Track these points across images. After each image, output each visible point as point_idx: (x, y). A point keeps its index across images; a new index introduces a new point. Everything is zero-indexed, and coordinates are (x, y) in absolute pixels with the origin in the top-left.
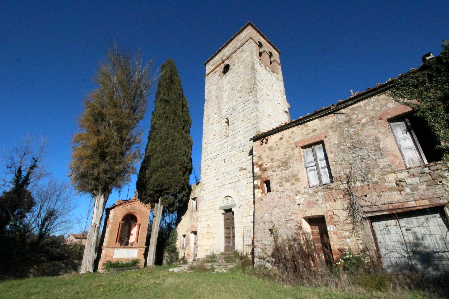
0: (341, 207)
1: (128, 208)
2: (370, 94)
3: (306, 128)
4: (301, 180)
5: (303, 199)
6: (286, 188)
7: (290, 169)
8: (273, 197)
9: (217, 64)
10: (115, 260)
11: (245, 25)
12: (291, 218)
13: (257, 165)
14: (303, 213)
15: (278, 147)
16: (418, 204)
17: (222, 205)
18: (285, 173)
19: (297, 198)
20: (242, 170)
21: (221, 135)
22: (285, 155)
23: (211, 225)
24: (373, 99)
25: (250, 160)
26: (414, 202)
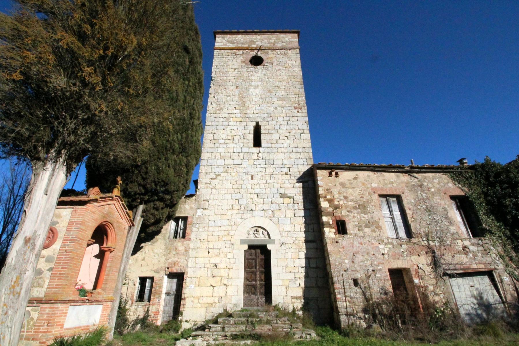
0: (425, 263)
1: (103, 211)
2: (439, 170)
6: (366, 234)
8: (352, 241)
9: (240, 45)
10: (72, 332)
11: (285, 30)
12: (379, 268)
13: (325, 199)
16: (479, 267)
17: (244, 237)
18: (364, 217)
19: (381, 246)
20: (285, 197)
24: (438, 175)
25: (299, 189)
26: (475, 265)
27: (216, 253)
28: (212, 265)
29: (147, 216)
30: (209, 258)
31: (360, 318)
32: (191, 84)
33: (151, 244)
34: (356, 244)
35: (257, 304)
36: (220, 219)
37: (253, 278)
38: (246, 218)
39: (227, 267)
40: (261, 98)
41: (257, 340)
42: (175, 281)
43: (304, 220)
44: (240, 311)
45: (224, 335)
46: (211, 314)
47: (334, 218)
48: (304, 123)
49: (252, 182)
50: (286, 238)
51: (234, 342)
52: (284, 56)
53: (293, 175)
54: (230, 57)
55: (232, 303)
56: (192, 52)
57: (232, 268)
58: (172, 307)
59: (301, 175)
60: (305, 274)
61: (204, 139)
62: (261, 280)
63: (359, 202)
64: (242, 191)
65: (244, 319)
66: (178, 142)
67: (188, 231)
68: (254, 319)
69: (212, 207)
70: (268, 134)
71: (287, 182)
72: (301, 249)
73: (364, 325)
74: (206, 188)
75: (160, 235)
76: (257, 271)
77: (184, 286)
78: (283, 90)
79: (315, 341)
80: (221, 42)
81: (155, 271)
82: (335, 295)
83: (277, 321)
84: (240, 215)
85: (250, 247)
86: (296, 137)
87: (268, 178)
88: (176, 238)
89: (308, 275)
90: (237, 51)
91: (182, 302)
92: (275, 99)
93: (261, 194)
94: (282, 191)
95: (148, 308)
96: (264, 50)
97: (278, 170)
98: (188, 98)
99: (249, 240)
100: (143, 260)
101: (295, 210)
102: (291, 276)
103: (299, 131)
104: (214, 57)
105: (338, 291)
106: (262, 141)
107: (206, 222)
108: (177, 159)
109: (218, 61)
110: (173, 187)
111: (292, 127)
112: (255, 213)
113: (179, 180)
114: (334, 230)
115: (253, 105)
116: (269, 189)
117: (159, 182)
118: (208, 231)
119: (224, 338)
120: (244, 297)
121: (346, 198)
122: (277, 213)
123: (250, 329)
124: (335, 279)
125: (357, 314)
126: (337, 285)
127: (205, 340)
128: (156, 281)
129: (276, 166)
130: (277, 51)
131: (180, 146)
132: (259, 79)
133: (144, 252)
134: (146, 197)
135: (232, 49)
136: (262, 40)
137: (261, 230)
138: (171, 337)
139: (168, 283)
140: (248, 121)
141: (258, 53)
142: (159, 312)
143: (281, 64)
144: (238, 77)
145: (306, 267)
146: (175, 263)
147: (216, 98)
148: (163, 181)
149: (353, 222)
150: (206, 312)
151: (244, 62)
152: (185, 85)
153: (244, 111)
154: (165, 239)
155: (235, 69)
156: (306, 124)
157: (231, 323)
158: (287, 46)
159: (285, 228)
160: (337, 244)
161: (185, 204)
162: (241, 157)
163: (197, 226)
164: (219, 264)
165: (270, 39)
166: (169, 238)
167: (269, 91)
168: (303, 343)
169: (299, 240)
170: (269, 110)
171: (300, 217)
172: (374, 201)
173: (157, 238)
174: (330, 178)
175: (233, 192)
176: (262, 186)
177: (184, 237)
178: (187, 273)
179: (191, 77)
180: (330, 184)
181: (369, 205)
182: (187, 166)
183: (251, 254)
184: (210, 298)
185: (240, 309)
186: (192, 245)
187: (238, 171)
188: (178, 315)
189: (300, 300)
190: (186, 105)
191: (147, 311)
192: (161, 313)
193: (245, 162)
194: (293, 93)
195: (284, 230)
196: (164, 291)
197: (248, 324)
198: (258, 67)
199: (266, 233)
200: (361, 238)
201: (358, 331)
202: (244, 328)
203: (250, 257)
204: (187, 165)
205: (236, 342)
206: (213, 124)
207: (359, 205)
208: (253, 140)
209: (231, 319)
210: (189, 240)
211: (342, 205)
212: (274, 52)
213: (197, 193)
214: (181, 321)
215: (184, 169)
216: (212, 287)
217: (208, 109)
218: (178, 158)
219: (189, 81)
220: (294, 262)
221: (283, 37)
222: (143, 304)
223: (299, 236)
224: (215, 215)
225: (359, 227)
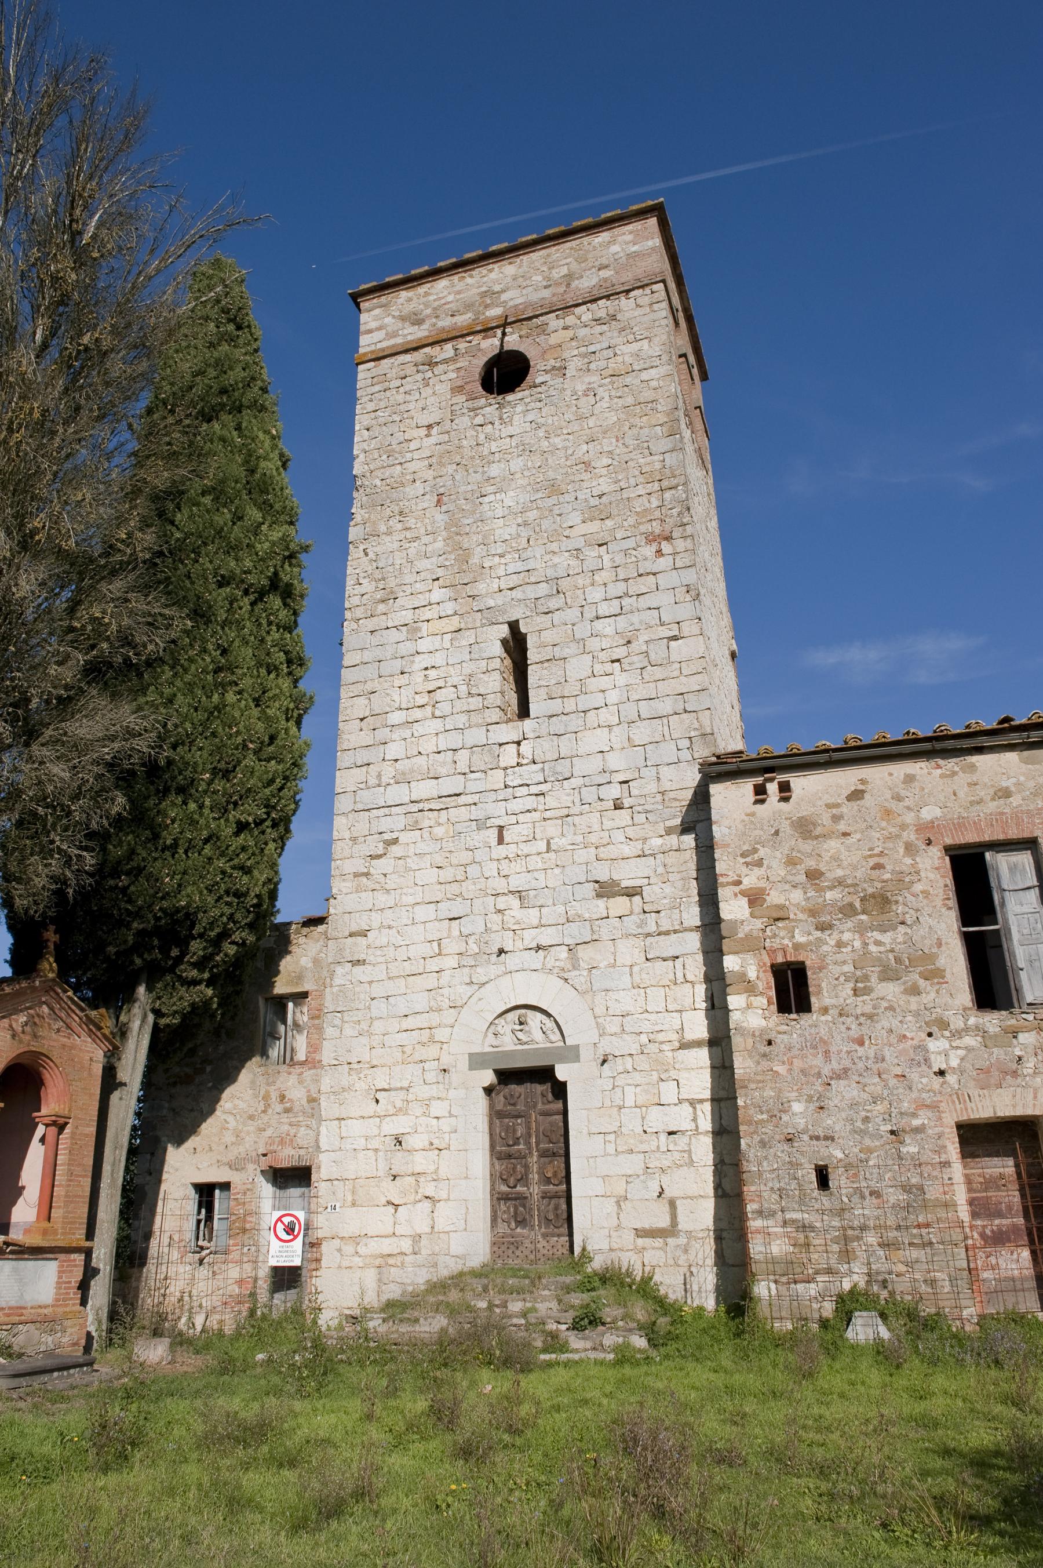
3: (969, 778)
4: (948, 976)
5: (961, 1053)
7: (901, 929)
9: (446, 322)
12: (916, 1122)
14: (958, 1106)
15: (842, 827)
18: (878, 943)
19: (934, 1045)
20: (613, 895)
21: (475, 703)
22: (873, 868)
23: (413, 1142)
38: (484, 979)
39: (432, 1144)
49: (501, 851)
52: (605, 328)
53: (640, 809)
61: (341, 718)
74: (357, 892)
84: (466, 970)
85: (506, 1076)
94: (603, 873)
104: (359, 394)
107: (361, 1006)
109: (371, 407)
112: (510, 961)
147: (371, 555)
155: (429, 427)
162: (462, 766)
163: (337, 1022)
169: (662, 1043)
184: (387, 1241)
198: (510, 397)
212: (570, 320)
216: (391, 1209)
220: (643, 1118)
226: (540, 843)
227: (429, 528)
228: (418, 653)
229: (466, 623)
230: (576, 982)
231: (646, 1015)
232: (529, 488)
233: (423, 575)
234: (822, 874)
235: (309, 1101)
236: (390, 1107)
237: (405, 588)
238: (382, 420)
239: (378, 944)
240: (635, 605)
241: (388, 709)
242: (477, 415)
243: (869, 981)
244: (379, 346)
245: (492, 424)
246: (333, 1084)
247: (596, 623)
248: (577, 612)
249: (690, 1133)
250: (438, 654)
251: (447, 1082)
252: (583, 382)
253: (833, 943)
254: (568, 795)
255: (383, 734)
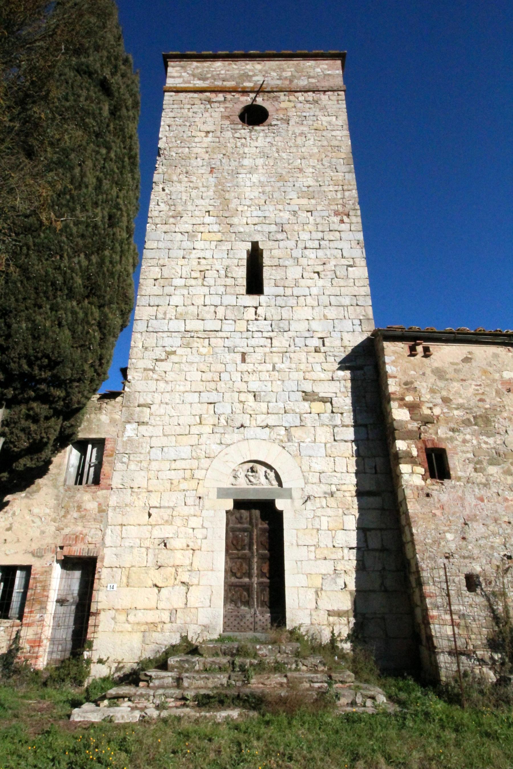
6: (492, 479)
8: (460, 493)
9: (219, 83)
13: (402, 403)
17: (227, 483)
18: (486, 443)
20: (314, 400)
25: (343, 382)
27: (166, 517)
28: (157, 542)
29: (12, 433)
30: (150, 527)
31: (482, 661)
32: (112, 155)
33: (26, 497)
34: (471, 500)
35: (252, 627)
36: (173, 444)
37: (244, 571)
38: (229, 442)
39: (188, 546)
40: (263, 193)
41: (254, 708)
42: (77, 574)
43: (355, 448)
44: (217, 641)
45: (180, 696)
46: (153, 646)
47: (420, 445)
48: (354, 244)
49: (243, 367)
50: (314, 486)
51: (203, 714)
52: (312, 106)
53: (331, 354)
54: (199, 107)
55: (199, 623)
56: (116, 94)
57: (200, 549)
58: (71, 631)
59: (347, 353)
60: (358, 564)
61: (141, 276)
62: (261, 574)
63: (475, 410)
64: (221, 386)
65: (224, 660)
66: (81, 272)
67: (106, 468)
68: (248, 661)
69: (158, 419)
70: (279, 268)
71: (318, 368)
72: (348, 509)
73: (492, 677)
74: (145, 380)
75: (45, 477)
76: (253, 556)
77: (95, 586)
78: (311, 175)
79: (386, 714)
80: (180, 77)
81: (33, 554)
82: (425, 610)
83: (297, 665)
84: (218, 435)
85: (239, 504)
86: (338, 273)
87: (276, 359)
88: (81, 483)
89: (363, 564)
90: (212, 96)
91: (91, 621)
92: (293, 195)
93: (263, 394)
94: (308, 387)
95: (18, 632)
96: (269, 92)
97: (300, 342)
98: (106, 184)
99: (236, 489)
100: (9, 529)
101: (335, 426)
102: (327, 567)
103: (345, 262)
104: (164, 107)
105: (433, 600)
106: (266, 282)
107: (143, 451)
108: (78, 310)
109: (172, 115)
110: (69, 371)
111: (328, 252)
112: (249, 433)
113: (84, 355)
114: (422, 470)
115: (246, 208)
116: (279, 383)
117: (37, 358)
118: (149, 470)
119: (179, 703)
120: (225, 611)
121: (446, 400)
122: (296, 433)
123: (239, 684)
124: (425, 575)
125: (474, 652)
126: (428, 589)
127: (136, 708)
128: (35, 574)
129: (295, 334)
130: (297, 94)
131: (87, 283)
132: (260, 152)
133: (11, 512)
134: (10, 393)
135: (202, 91)
136: (266, 72)
137: (261, 470)
138: (64, 698)
139: (61, 578)
140: (236, 241)
141: (257, 99)
142: (40, 641)
143: (305, 122)
144: (214, 148)
145: (358, 548)
146: (76, 537)
147: (167, 191)
148: (47, 356)
149: (463, 452)
150: (143, 642)
151: (228, 117)
152: (99, 157)
153: (228, 219)
154: (55, 486)
155: (208, 132)
156: (358, 247)
157: (197, 667)
158: (318, 84)
159: (312, 465)
160: (428, 499)
161: (101, 413)
162: (220, 315)
163: (125, 460)
164: (171, 540)
165: (284, 70)
166: (64, 485)
167: (281, 178)
168: (360, 720)
169: (345, 491)
170: (281, 217)
171: (346, 441)
172: (507, 408)
173: (38, 483)
174: (412, 358)
175: (202, 389)
176: (265, 376)
177: (96, 481)
178: (103, 558)
179: (114, 142)
180: (413, 372)
181: (498, 416)
182: (101, 326)
183: (240, 520)
184: (151, 613)
185: (216, 636)
186: (113, 500)
187: (213, 345)
188: (83, 647)
189: (345, 619)
190: (100, 197)
191: (16, 638)
192: (46, 643)
193: (228, 326)
194: (331, 183)
195: (312, 470)
196: (53, 595)
197: (233, 671)
198: (257, 128)
199: (272, 475)
200: (481, 486)
201: (481, 692)
202: (224, 681)
203: (239, 526)
204: (103, 324)
205: (208, 714)
206: (160, 247)
207: (475, 417)
208: (245, 280)
209: (195, 659)
210: (107, 489)
211: (438, 417)
212: (292, 98)
213: (126, 389)
214: (89, 661)
215: (94, 331)
216: (156, 590)
217: (149, 215)
218: (81, 308)
219: (109, 149)
220: (333, 538)
221: (310, 66)
222: (8, 625)
223: (343, 482)
224: (164, 435)
225: (477, 463)
226: (268, 365)
227: (205, 184)
228: (194, 249)
229: (226, 238)
230: (290, 449)
231: (335, 474)
232: (267, 175)
233: (200, 208)
234: (451, 400)
235: (99, 512)
236: (159, 519)
237: (188, 212)
238: (177, 123)
239: (158, 413)
240: (328, 245)
241: (173, 276)
242: (236, 132)
243: (483, 464)
244: (178, 85)
245: (245, 138)
246: (118, 500)
247: (305, 251)
248: (293, 243)
249: (363, 549)
250: (207, 251)
251: (201, 504)
252: (299, 129)
253: (461, 440)
254: (287, 341)
255: (168, 290)
